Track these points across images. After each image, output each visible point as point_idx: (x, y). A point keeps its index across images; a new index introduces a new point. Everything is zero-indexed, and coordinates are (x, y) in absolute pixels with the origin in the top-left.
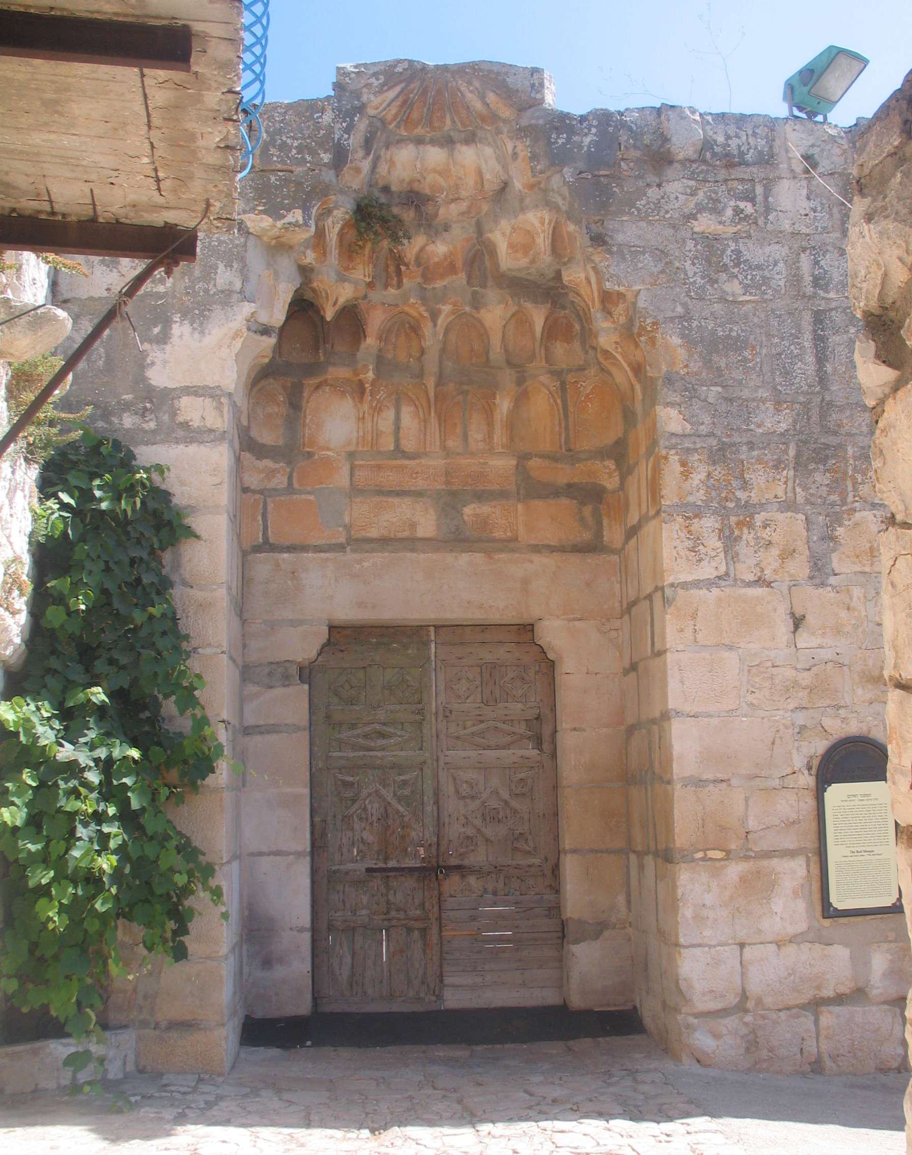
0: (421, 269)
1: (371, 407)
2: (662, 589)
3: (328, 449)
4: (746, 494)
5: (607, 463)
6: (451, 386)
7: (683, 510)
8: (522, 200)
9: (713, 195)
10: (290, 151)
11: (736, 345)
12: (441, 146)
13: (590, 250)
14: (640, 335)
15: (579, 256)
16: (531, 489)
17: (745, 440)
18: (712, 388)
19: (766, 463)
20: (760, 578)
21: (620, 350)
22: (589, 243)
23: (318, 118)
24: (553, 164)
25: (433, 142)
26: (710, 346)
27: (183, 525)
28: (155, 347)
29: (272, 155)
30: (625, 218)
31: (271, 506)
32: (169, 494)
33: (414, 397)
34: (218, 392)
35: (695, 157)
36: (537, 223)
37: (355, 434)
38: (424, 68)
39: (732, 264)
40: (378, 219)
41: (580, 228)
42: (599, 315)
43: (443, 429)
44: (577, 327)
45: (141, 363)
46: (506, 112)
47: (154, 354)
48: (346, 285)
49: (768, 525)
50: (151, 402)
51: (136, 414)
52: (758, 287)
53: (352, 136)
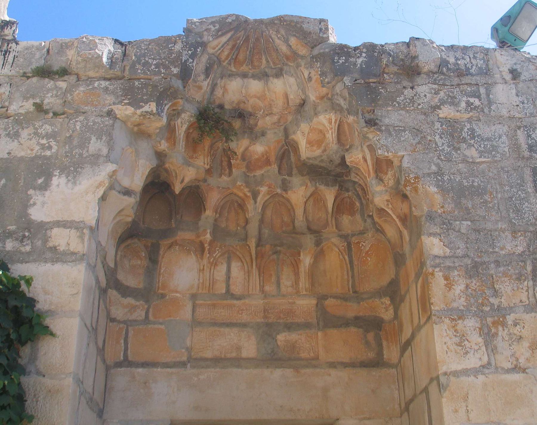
0: (245, 163)
1: (209, 262)
2: (437, 378)
3: (177, 292)
4: (498, 300)
5: (383, 300)
6: (268, 247)
7: (449, 313)
8: (315, 109)
9: (450, 94)
10: (151, 66)
11: (479, 192)
12: (259, 79)
13: (365, 129)
14: (405, 186)
15: (357, 142)
16: (327, 321)
17: (492, 259)
18: (463, 222)
19: (511, 276)
20: (516, 366)
21: (390, 206)
22: (364, 125)
23: (171, 47)
24: (336, 75)
25: (254, 77)
26: (459, 193)
27: (43, 325)
28: (38, 192)
29: (138, 69)
30: (390, 109)
31: (130, 334)
32: (35, 301)
33: (241, 256)
34: (82, 225)
35: (436, 70)
36: (325, 122)
37: (197, 281)
38: (246, 21)
39: (469, 137)
40: (214, 123)
41: (358, 118)
42: (374, 182)
43: (261, 278)
44: (358, 204)
45: (26, 204)
46: (303, 51)
47: (37, 198)
48: (191, 168)
49: (518, 324)
50: (29, 231)
51: (17, 239)
52: (490, 152)
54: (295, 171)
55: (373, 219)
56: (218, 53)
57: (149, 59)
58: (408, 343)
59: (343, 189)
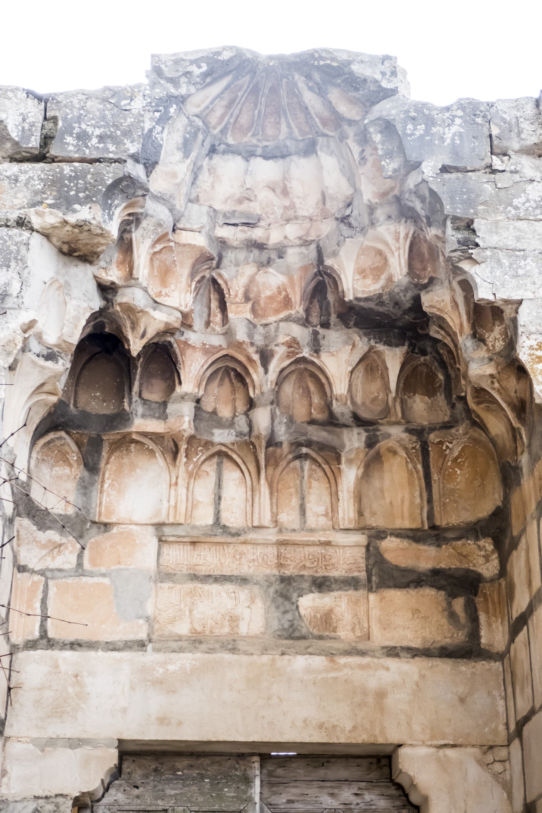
0: (249, 305)
5: (482, 543)
15: (442, 274)
21: (496, 385)
23: (125, 105)
29: (68, 144)
43: (274, 500)
44: (441, 377)
53: (166, 131)
54: (333, 318)
55: (466, 403)
56: (204, 114)
57: (88, 125)
58: (523, 620)
59: (416, 351)
